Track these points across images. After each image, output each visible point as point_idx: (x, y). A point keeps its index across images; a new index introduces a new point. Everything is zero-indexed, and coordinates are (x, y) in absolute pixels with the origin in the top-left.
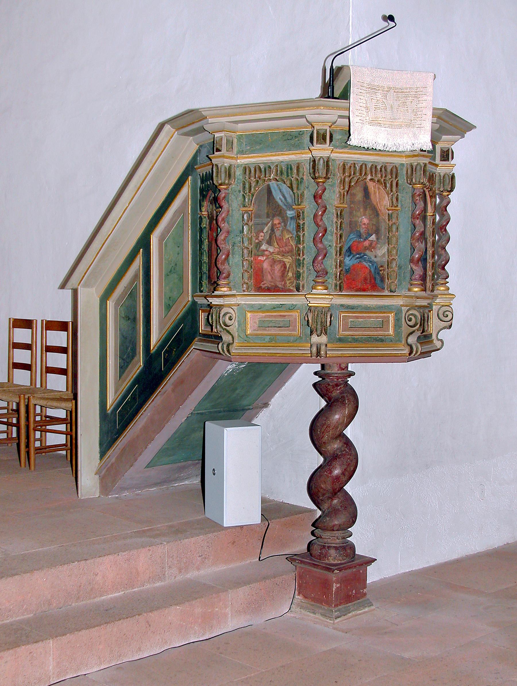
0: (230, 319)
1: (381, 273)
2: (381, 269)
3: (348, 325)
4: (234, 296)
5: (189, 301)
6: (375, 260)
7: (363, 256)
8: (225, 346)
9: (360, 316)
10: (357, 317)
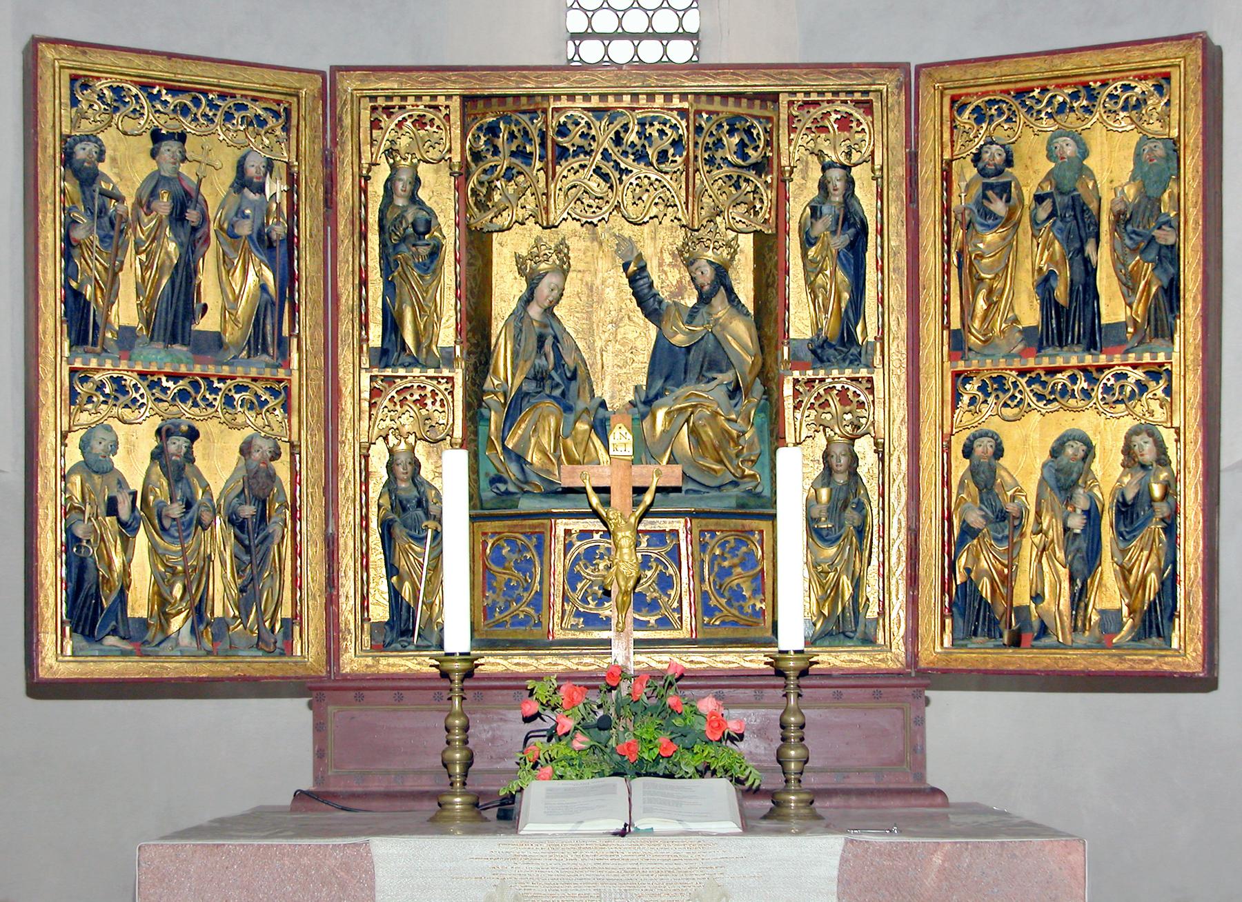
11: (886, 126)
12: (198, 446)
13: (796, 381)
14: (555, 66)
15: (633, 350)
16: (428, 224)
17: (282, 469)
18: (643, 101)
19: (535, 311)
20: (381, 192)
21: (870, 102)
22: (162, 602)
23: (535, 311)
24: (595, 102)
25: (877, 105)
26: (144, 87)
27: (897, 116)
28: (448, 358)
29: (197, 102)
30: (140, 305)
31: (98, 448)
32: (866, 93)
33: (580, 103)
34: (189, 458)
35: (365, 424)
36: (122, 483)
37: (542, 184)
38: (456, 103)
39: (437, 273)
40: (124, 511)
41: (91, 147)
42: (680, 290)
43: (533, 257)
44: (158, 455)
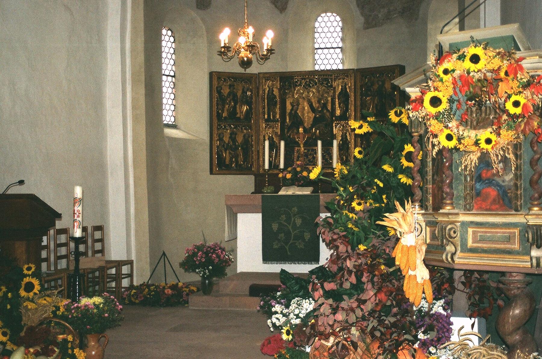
0: (455, 232)
1: (509, 195)
2: (509, 191)
3: (477, 239)
4: (457, 214)
5: (437, 219)
6: (503, 184)
7: (492, 181)
8: (449, 256)
9: (489, 232)
10: (486, 232)
11: (351, 80)
12: (237, 136)
13: (335, 123)
14: (210, 155)
15: (311, 118)
16: (275, 97)
17: (250, 140)
18: (310, 77)
19: (293, 112)
20: (267, 92)
21: (348, 75)
22: (231, 162)
23: (293, 112)
24: (302, 77)
25: (349, 76)
26: (229, 78)
27: (353, 78)
28: (278, 121)
29: (237, 80)
30: (228, 113)
31: (221, 136)
32: (347, 74)
33: (299, 77)
34: (235, 138)
35: (264, 132)
36: (225, 142)
37: (293, 91)
38: (279, 78)
39: (276, 107)
40: (225, 147)
41: (220, 88)
42: (318, 108)
43: (292, 102)
44: (230, 138)
